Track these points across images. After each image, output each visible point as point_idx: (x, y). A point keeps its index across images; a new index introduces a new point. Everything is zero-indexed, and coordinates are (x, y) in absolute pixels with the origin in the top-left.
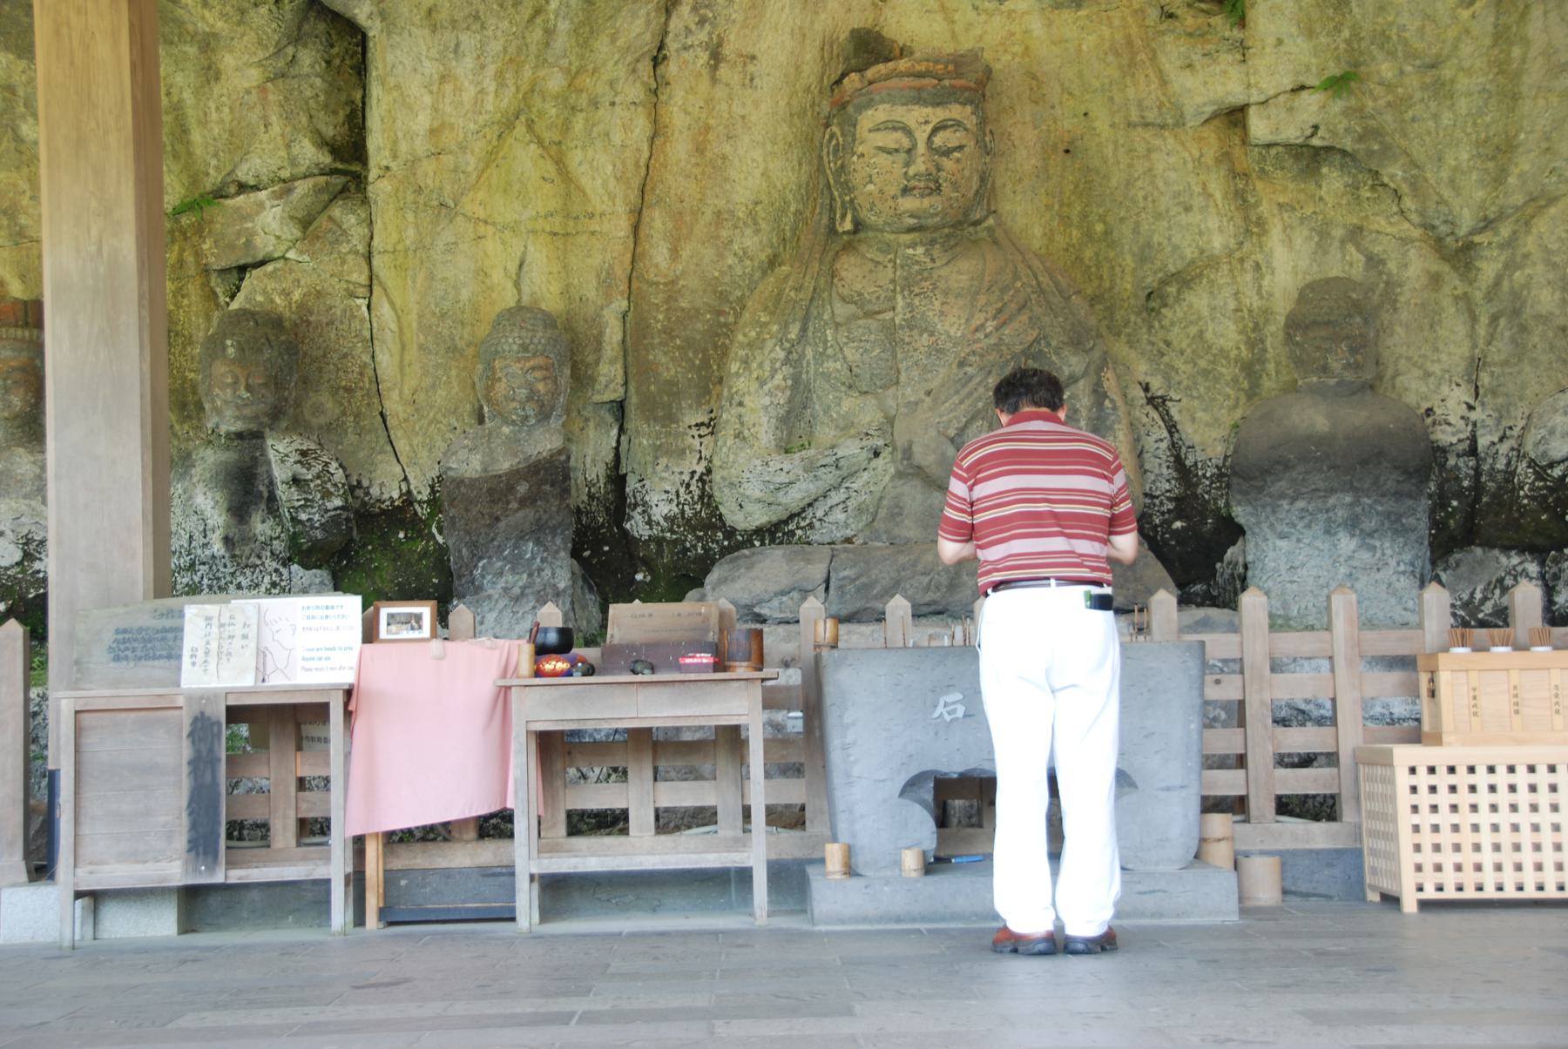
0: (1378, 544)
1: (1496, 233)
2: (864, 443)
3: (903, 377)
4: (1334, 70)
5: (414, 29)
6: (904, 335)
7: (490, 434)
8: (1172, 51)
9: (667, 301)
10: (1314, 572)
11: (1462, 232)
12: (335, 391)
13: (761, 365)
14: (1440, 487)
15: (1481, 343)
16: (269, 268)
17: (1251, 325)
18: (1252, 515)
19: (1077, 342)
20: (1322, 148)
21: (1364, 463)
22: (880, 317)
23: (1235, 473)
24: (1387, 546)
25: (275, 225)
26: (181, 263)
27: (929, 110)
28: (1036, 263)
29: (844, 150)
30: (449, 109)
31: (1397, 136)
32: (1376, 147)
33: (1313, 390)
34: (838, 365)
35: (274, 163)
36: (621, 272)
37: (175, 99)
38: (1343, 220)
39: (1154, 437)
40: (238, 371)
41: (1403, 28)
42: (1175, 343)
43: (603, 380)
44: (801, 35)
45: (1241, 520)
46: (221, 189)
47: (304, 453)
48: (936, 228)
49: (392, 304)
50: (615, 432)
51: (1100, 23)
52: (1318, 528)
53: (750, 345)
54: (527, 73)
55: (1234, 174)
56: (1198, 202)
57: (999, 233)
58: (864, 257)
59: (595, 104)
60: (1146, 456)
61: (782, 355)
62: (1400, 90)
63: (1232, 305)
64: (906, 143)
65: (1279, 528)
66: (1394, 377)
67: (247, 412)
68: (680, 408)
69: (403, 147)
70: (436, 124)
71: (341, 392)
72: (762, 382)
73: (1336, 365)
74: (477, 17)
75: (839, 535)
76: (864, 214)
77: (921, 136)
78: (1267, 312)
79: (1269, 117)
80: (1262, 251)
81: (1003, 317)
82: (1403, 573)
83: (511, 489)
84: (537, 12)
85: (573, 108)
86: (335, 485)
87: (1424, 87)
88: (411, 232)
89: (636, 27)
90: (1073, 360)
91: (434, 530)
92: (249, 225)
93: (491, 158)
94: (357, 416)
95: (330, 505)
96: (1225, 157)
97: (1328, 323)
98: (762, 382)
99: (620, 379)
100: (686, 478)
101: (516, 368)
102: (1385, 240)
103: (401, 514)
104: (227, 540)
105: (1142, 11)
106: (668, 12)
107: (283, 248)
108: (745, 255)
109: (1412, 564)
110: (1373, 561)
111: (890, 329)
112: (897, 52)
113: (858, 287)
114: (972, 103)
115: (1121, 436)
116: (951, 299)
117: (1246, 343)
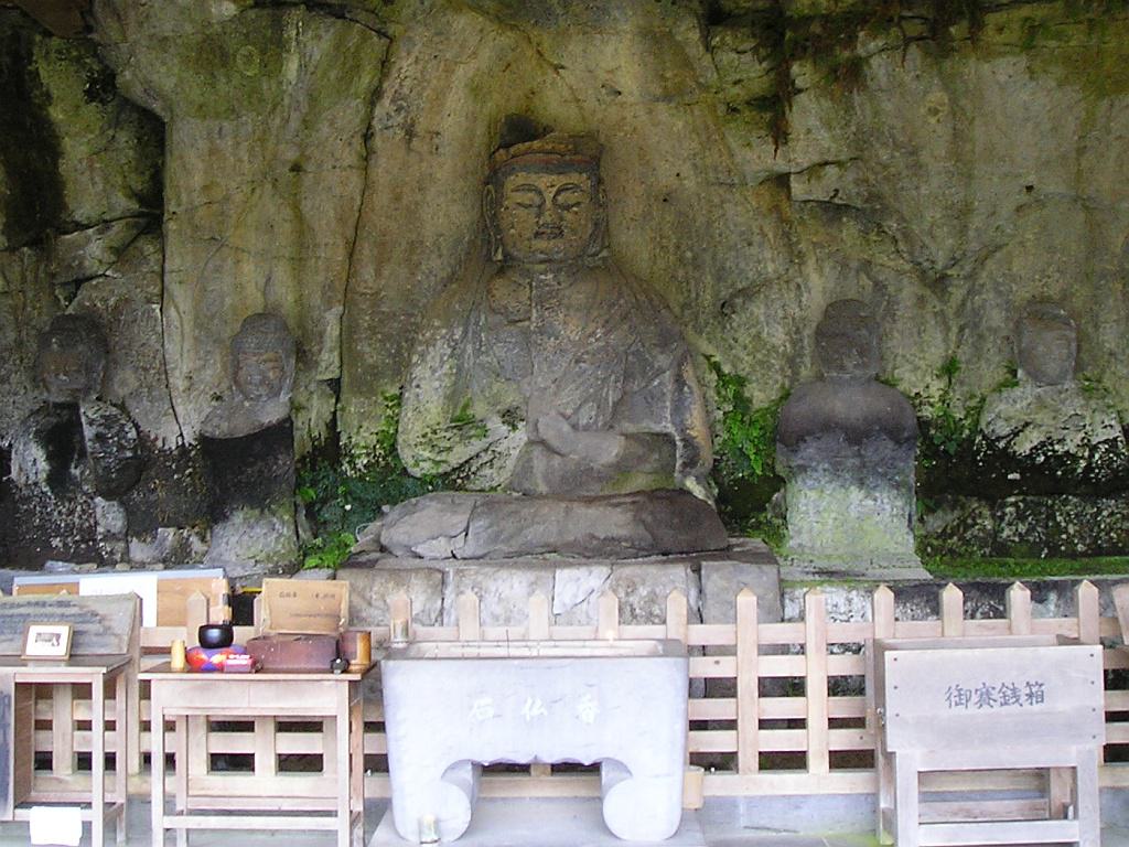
0: (877, 494)
1: (962, 268)
11: (939, 266)
15: (953, 346)
16: (94, 282)
20: (842, 205)
22: (520, 324)
25: (98, 253)
29: (497, 203)
31: (892, 200)
43: (323, 364)
55: (782, 220)
56: (757, 239)
61: (449, 351)
62: (893, 169)
63: (781, 313)
64: (537, 200)
69: (184, 197)
72: (434, 371)
74: (233, 111)
77: (549, 196)
80: (801, 276)
81: (609, 327)
82: (896, 515)
94: (150, 388)
99: (337, 363)
102: (887, 271)
109: (903, 509)
111: (526, 333)
112: (541, 130)
115: (695, 413)
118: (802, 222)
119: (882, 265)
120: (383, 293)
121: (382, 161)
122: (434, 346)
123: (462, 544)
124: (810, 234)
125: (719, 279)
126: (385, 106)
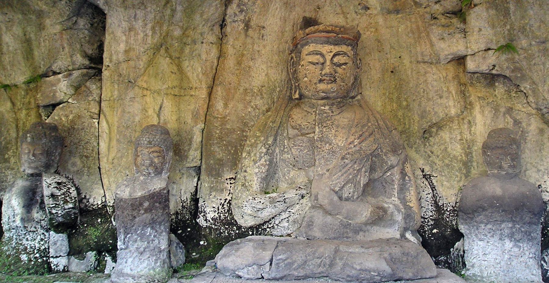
0: (521, 245)
2: (298, 192)
4: (503, 42)
6: (318, 144)
7: (135, 179)
8: (436, 31)
9: (221, 125)
10: (494, 256)
12: (81, 157)
13: (255, 155)
14: (545, 219)
16: (61, 106)
17: (467, 146)
18: (468, 229)
19: (394, 151)
20: (496, 75)
21: (517, 209)
22: (308, 136)
23: (461, 211)
24: (525, 246)
25: (64, 89)
26: (29, 103)
27: (332, 47)
28: (378, 116)
30: (132, 42)
33: (494, 175)
35: (66, 63)
36: (202, 113)
37: (28, 37)
38: (504, 105)
39: (426, 192)
40: (30, 148)
41: (531, 26)
42: (435, 152)
43: (191, 158)
44: (285, 20)
45: (462, 231)
46: (46, 74)
47: (59, 184)
49: (107, 122)
50: (196, 179)
51: (407, 20)
52: (496, 238)
53: (251, 146)
54: (165, 28)
55: (461, 84)
56: (445, 95)
57: (362, 103)
58: (303, 109)
59: (194, 42)
60: (422, 200)
61: (265, 151)
64: (321, 60)
66: (525, 171)
67: (32, 165)
68: (223, 171)
69: (114, 58)
70: (127, 48)
71: (84, 157)
72: (255, 162)
73: (505, 165)
74: (143, 4)
75: (284, 233)
77: (328, 57)
78: (473, 141)
79: (475, 61)
81: (362, 138)
82: (531, 258)
83: (141, 204)
85: (185, 43)
86: (71, 198)
87: (539, 51)
88: (116, 93)
89: (212, 11)
90: (393, 158)
91: (112, 219)
92: (55, 88)
93: (150, 63)
94: (89, 168)
95: (66, 207)
96: (456, 77)
97: (502, 147)
98: (255, 162)
100: (223, 202)
101: (146, 151)
103: (102, 212)
104: (22, 220)
105: (423, 15)
106: (226, 6)
107: (67, 98)
108: (256, 107)
109: (535, 254)
110: (520, 252)
111: (312, 141)
113: (299, 122)
114: (351, 45)
116: (340, 129)
117: (465, 154)
118: (472, 84)
119: (518, 110)
120: (228, 118)
121: (231, 41)
122: (256, 147)
123: (268, 270)
124: (476, 93)
125: (422, 117)
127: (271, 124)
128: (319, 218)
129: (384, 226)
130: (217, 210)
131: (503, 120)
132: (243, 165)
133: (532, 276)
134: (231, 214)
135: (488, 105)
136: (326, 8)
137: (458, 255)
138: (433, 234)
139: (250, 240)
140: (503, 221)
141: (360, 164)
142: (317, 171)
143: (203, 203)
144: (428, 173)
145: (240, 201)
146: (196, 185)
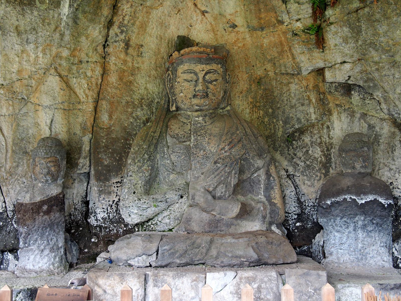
0: (373, 235)
3: (193, 167)
5: (11, 33)
6: (194, 150)
14: (396, 212)
17: (326, 149)
20: (352, 84)
22: (184, 143)
24: (376, 235)
27: (204, 66)
29: (173, 80)
31: (379, 81)
32: (372, 85)
34: (169, 162)
39: (289, 191)
43: (81, 165)
48: (207, 110)
50: (86, 184)
55: (319, 93)
57: (231, 112)
58: (179, 120)
63: (319, 140)
65: (336, 228)
66: (379, 170)
68: (110, 176)
74: (34, 29)
76: (180, 104)
77: (201, 75)
80: (330, 121)
81: (232, 145)
82: (383, 246)
84: (56, 28)
100: (111, 203)
106: (109, 29)
109: (386, 243)
111: (188, 148)
115: (276, 191)
116: (212, 137)
120: (113, 128)
123: (154, 259)
126: (115, 29)
127: (152, 134)
128: (196, 214)
129: (252, 221)
130: (106, 211)
131: (358, 124)
132: (129, 170)
133: (383, 262)
134: (119, 214)
135: (344, 112)
136: (197, 26)
137: (318, 245)
138: (297, 228)
139: (138, 235)
140: (356, 215)
141: (230, 167)
142: (193, 174)
143: (93, 205)
144: (292, 173)
145: (127, 202)
146: (85, 189)
